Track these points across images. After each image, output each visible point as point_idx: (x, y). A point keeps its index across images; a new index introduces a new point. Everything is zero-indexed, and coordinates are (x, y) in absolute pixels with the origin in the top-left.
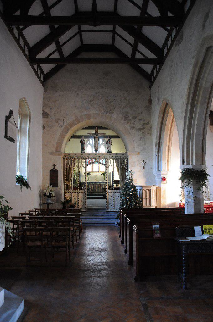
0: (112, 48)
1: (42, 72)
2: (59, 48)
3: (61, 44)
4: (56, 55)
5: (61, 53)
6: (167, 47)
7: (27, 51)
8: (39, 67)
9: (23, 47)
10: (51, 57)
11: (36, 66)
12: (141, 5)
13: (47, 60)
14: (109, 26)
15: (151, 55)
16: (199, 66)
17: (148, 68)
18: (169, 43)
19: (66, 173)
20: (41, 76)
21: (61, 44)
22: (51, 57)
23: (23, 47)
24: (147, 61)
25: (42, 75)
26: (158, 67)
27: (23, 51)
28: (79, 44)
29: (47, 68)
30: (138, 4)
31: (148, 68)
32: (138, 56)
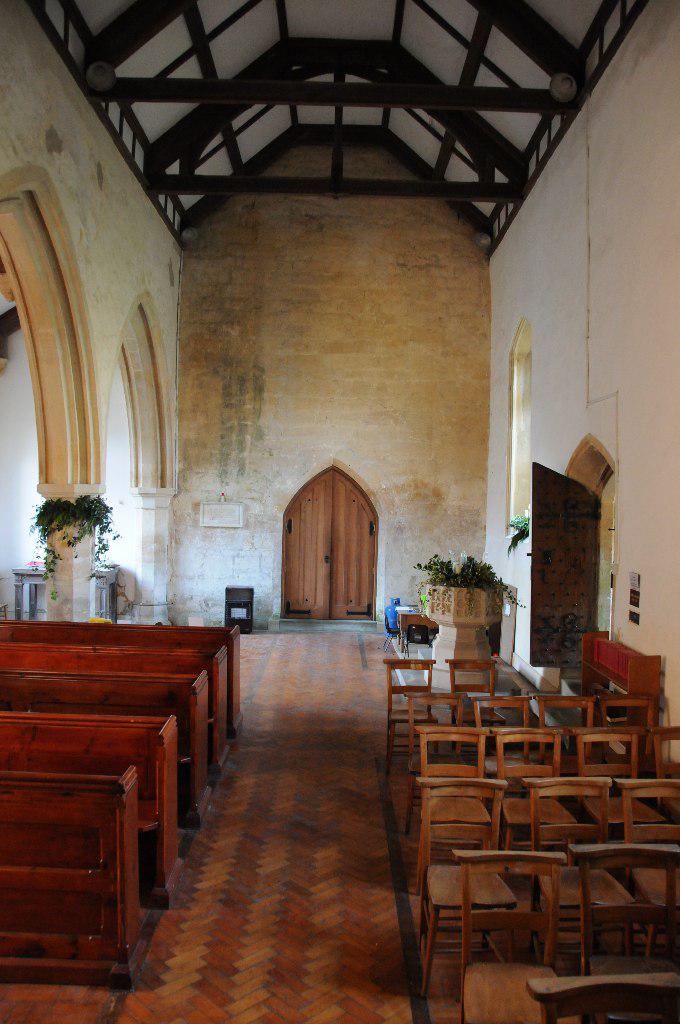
0: (381, 138)
1: (139, 133)
2: (201, 44)
3: (208, 28)
4: (190, 71)
5: (207, 64)
6: (538, 154)
7: (75, 47)
8: (128, 115)
9: (61, 33)
10: (175, 75)
11: (114, 111)
12: (468, 35)
13: (160, 88)
14: (372, 110)
15: (528, 73)
16: (50, 992)
17: (518, 127)
18: (543, 146)
19: (504, 910)
20: (134, 150)
21: (208, 28)
22: (175, 75)
23: (61, 33)
24: (514, 98)
25: (138, 145)
26: (556, 122)
27: (60, 45)
28: (288, 124)
29: (157, 117)
30: (461, 30)
31: (518, 127)
32: (485, 79)
